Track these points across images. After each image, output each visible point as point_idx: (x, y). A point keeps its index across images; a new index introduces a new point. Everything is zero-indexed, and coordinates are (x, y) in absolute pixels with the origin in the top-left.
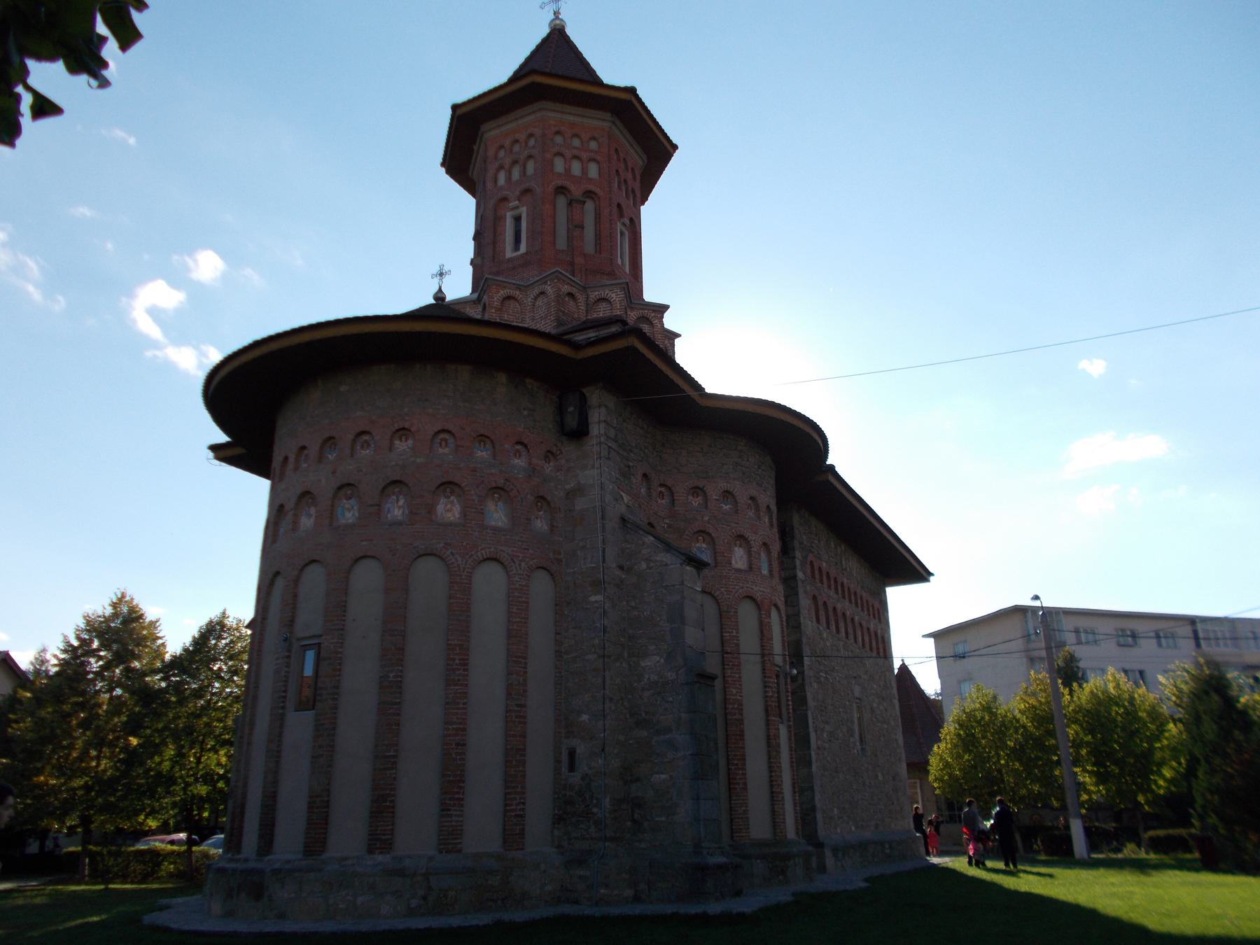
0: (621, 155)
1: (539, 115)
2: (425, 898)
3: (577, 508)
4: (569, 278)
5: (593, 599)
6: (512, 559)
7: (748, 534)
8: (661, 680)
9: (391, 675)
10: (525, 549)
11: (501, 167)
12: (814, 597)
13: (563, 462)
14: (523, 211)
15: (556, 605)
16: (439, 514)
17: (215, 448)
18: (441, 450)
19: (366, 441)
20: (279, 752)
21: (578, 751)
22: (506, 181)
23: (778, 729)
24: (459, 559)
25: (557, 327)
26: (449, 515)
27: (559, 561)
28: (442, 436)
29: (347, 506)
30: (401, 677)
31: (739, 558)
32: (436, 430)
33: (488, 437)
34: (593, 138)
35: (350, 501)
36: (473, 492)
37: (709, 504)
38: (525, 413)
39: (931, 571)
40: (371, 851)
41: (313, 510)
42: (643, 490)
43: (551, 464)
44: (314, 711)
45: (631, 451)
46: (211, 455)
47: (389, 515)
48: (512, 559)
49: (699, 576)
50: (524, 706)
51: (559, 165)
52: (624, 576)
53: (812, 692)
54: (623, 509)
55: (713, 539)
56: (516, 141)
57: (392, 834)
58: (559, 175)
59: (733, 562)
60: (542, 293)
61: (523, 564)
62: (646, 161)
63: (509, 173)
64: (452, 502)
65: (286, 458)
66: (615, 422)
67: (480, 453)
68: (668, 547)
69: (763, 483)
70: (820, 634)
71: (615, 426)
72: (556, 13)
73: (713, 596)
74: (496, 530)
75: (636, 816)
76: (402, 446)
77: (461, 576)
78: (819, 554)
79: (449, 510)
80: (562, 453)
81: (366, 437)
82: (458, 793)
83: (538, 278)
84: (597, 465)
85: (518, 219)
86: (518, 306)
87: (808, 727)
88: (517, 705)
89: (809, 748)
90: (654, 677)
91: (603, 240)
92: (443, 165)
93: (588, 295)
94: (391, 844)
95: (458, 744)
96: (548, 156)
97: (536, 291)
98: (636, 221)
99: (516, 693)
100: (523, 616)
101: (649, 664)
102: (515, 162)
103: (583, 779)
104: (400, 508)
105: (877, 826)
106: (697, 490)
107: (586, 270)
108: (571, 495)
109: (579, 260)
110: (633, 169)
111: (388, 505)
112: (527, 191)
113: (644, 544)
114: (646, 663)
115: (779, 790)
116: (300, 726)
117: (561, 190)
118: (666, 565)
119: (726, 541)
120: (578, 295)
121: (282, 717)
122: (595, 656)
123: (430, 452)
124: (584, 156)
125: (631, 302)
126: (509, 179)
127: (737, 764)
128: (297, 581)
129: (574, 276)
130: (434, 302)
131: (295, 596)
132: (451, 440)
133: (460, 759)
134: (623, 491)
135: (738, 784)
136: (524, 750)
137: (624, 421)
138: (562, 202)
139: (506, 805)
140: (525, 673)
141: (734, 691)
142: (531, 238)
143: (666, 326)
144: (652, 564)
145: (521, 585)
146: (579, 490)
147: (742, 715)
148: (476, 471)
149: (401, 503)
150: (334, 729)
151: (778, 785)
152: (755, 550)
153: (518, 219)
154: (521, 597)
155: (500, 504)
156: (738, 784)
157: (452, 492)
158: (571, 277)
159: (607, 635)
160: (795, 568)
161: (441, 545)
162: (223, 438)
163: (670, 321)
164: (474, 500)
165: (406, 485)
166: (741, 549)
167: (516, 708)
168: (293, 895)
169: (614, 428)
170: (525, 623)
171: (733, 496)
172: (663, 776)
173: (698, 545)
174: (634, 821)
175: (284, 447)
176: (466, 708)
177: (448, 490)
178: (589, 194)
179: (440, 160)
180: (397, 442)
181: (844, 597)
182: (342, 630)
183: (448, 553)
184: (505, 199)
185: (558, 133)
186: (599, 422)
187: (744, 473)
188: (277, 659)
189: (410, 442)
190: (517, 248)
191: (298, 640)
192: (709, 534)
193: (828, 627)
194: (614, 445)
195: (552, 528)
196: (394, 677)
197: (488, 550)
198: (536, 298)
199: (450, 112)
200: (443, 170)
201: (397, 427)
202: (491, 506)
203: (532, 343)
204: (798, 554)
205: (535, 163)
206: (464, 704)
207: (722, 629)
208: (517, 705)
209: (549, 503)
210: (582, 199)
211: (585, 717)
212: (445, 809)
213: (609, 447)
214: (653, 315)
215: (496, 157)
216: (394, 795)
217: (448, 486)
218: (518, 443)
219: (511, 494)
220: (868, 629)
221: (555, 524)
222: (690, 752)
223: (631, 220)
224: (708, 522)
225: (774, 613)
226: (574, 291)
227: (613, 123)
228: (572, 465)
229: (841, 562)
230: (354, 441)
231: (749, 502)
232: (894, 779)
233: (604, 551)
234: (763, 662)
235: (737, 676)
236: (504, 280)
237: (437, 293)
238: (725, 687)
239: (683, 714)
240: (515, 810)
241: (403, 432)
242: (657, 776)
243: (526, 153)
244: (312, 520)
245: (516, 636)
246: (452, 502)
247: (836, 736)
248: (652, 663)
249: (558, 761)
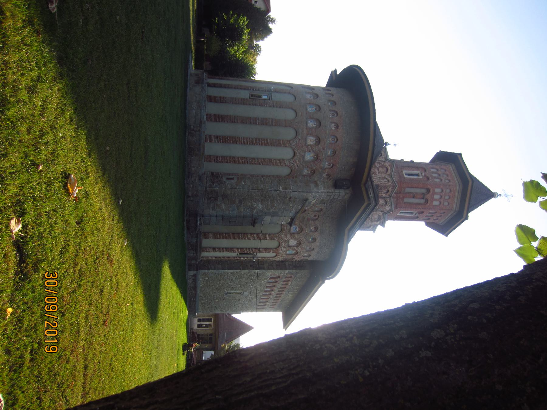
0: (443, 215)
1: (457, 184)
2: (193, 130)
3: (311, 184)
4: (394, 191)
5: (281, 187)
6: (294, 161)
7: (300, 247)
8: (254, 208)
9: (259, 121)
10: (298, 165)
11: (438, 170)
12: (279, 277)
13: (327, 181)
14: (421, 177)
15: (279, 176)
16: (310, 137)
17: (335, 71)
18: (331, 139)
19: (334, 115)
20: (237, 88)
21: (233, 181)
22: (432, 171)
23: (236, 252)
24: (295, 143)
25: (376, 185)
26: (309, 141)
27: (293, 178)
28: (336, 139)
29: (313, 108)
30: (258, 124)
31: (293, 242)
32: (338, 137)
33: (335, 154)
34: (449, 204)
35: (315, 109)
36: (317, 148)
37: (312, 233)
38: (343, 168)
39: (287, 329)
40: (207, 115)
41: (312, 98)
42: (317, 209)
43: (326, 177)
44: (249, 98)
45: (330, 204)
46: (333, 70)
47: (309, 122)
48: (294, 161)
49: (287, 224)
51: (438, 190)
52: (288, 199)
54: (310, 200)
55: (300, 233)
56: (448, 176)
57: (212, 121)
58: (434, 190)
59: (292, 240)
60: (389, 181)
61: (293, 165)
62: (441, 225)
63: (435, 173)
64: (313, 142)
65: (330, 90)
66: (340, 199)
67: (329, 151)
68: (297, 213)
69: (319, 254)
70: (266, 279)
71: (339, 198)
72: (500, 195)
73: (280, 232)
74: (304, 156)
75: (212, 198)
76: (333, 126)
77: (289, 144)
78: (294, 280)
79: (311, 140)
80: (330, 180)
81: (336, 115)
82: (222, 141)
83: (395, 181)
84: (325, 191)
85: (418, 175)
86: (384, 173)
87: (235, 269)
88: (248, 161)
89: (229, 269)
90: (255, 206)
91: (410, 206)
92: (440, 151)
93: (388, 198)
94: (209, 121)
95: (237, 141)
96: (442, 186)
97: (389, 179)
98: (418, 219)
99: (251, 161)
100: (276, 164)
101: (259, 205)
102: (439, 175)
103: (224, 182)
104: (312, 125)
105: (201, 296)
106: (316, 229)
107: (398, 198)
108: (316, 183)
109: (401, 196)
110: (437, 219)
111: (313, 121)
112: (428, 179)
113: (298, 206)
114: (259, 204)
115: (217, 251)
116: (244, 94)
117: (428, 191)
118: (291, 212)
119: (299, 238)
120: (388, 194)
121: (248, 89)
122: (262, 187)
123: (330, 135)
124: (442, 200)
125: (385, 214)
126: (433, 173)
127: (225, 236)
128: (289, 93)
129: (394, 193)
130: (385, 142)
131: (285, 93)
132: (334, 142)
133: (232, 142)
134: (316, 200)
135: (219, 236)
136: (234, 163)
137: (340, 202)
138: (423, 191)
139: (218, 156)
140: (258, 164)
141: (249, 237)
142: (410, 179)
144: (291, 208)
145: (286, 163)
146: (316, 185)
147: (241, 239)
148: (323, 149)
149: (314, 125)
150: (243, 104)
151: (218, 251)
152: (296, 248)
153: (418, 175)
154: (282, 164)
155: (313, 158)
156: (219, 236)
157: (316, 142)
158: (394, 192)
159: (269, 191)
160: (290, 269)
161: (299, 138)
162: (338, 73)
163: (379, 227)
164: (314, 149)
165: (319, 127)
166: (296, 243)
167: (247, 161)
168: (196, 92)
169: (338, 198)
170: (274, 165)
171: (314, 242)
172: (224, 207)
173: (298, 228)
174: (210, 198)
175: (333, 90)
176: (248, 144)
177: (317, 141)
178: (427, 201)
180: (334, 125)
181: (279, 291)
182: (274, 107)
183: (297, 140)
185: (451, 191)
186: (340, 193)
187: (322, 246)
188: (265, 88)
189: (334, 129)
190: (406, 174)
191: (271, 94)
192: (301, 232)
193: (269, 282)
194: (332, 198)
195: (305, 176)
196: (258, 122)
197: (297, 153)
198: (387, 179)
199: (459, 152)
200: (439, 152)
201: (339, 124)
202: (312, 154)
203: (366, 168)
204: (294, 271)
205: (439, 182)
206: (249, 144)
207: (270, 234)
208: (248, 161)
209: (312, 175)
210: (425, 198)
211: (243, 183)
212: (218, 137)
213: (331, 196)
214: (381, 222)
215: (441, 169)
216: (223, 122)
217: (319, 141)
218: (333, 165)
219: (316, 161)
220: (267, 301)
221: (306, 177)
222: (231, 215)
223: (418, 217)
224: (305, 232)
225: (274, 254)
226: (389, 193)
227: (455, 211)
228: (326, 183)
229: (291, 291)
230: (335, 111)
231: (312, 248)
232: (215, 307)
233: (296, 192)
234: (257, 248)
235: (254, 238)
236: (394, 168)
237: (388, 143)
238: (250, 234)
239: (243, 214)
240: (216, 159)
241: (337, 126)
242: (224, 205)
244: (309, 98)
245: (270, 162)
246: (313, 142)
247: (231, 282)
248: (259, 206)
249: (230, 174)
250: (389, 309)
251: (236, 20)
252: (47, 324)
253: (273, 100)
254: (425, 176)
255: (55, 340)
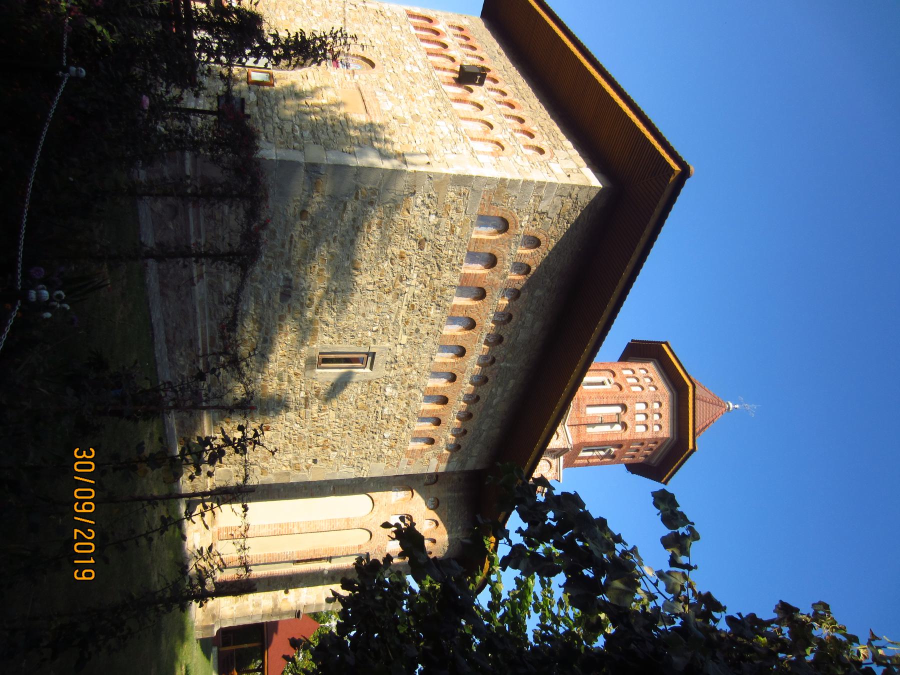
14: (608, 386)
50: (269, 525)
53: (297, 559)
85: (603, 383)
102: (638, 380)
117: (624, 407)
126: (628, 377)
143: (555, 494)
153: (603, 383)
179: (635, 339)
184: (614, 375)
243: (644, 386)
250: (607, 337)
251: (178, 456)
252: (78, 533)
253: (417, 68)
254: (615, 383)
255: (90, 560)
